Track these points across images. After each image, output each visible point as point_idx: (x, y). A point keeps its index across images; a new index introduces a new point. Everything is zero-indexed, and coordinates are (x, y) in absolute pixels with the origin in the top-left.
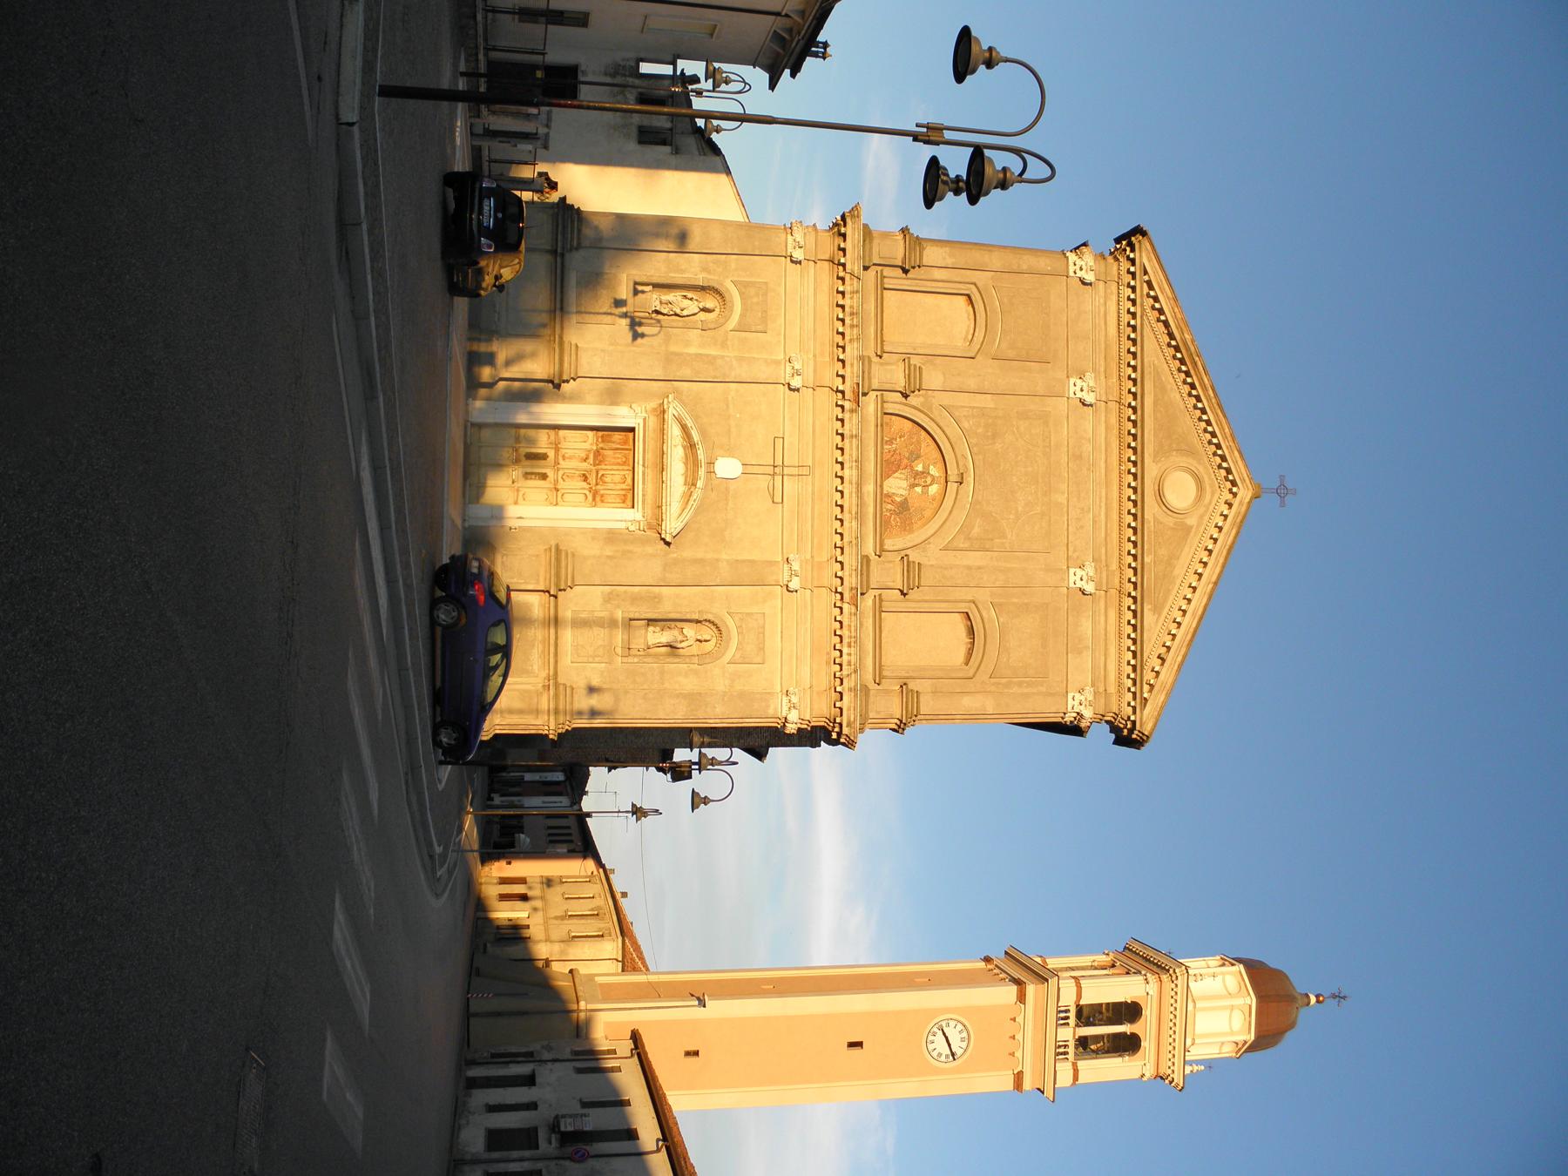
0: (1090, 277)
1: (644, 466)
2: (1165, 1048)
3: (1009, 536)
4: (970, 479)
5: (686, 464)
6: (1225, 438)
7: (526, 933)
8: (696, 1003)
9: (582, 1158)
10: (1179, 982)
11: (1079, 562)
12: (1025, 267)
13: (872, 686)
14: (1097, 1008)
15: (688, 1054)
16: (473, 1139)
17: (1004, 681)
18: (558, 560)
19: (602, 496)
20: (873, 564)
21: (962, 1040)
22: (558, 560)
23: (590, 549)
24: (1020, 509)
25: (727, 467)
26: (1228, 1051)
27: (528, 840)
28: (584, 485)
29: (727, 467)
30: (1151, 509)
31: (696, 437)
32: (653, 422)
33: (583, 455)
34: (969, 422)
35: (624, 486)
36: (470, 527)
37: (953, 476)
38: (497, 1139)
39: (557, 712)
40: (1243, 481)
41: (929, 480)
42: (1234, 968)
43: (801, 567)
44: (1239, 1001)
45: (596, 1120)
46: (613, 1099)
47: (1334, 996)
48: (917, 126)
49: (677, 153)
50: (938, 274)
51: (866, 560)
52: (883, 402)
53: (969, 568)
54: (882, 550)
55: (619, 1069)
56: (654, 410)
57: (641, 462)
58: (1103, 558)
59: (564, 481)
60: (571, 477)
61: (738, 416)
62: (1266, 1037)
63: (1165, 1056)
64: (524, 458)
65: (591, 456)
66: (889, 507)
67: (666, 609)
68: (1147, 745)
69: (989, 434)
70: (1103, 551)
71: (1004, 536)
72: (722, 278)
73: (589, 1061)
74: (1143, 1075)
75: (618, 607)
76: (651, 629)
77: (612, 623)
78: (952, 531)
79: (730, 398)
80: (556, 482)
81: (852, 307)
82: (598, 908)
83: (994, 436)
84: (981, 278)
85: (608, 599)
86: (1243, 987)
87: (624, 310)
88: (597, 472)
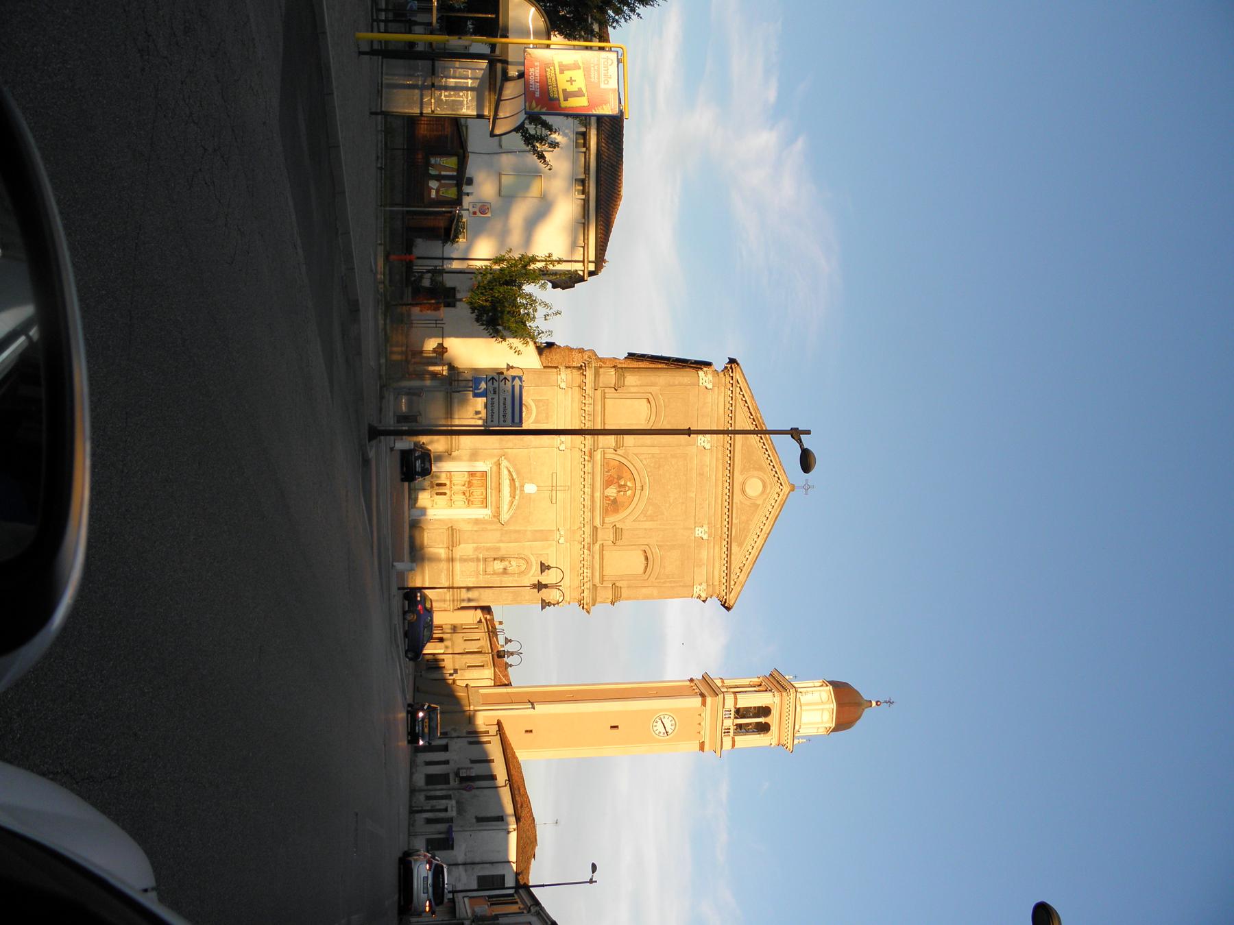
0: (710, 386)
2: (784, 730)
5: (511, 488)
6: (777, 463)
7: (442, 664)
8: (531, 706)
9: (469, 789)
10: (791, 696)
11: (701, 525)
12: (677, 383)
13: (598, 585)
14: (747, 709)
15: (527, 731)
16: (420, 780)
17: (662, 581)
18: (452, 534)
20: (599, 530)
21: (672, 725)
22: (452, 534)
23: (467, 527)
25: (530, 488)
26: (822, 731)
27: (469, 23)
28: (464, 496)
29: (530, 488)
30: (738, 497)
31: (515, 476)
32: (495, 468)
33: (463, 483)
35: (482, 497)
36: (412, 520)
37: (638, 487)
38: (431, 779)
39: (453, 601)
40: (785, 483)
41: (627, 488)
42: (828, 688)
43: (565, 533)
44: (827, 706)
45: (477, 770)
46: (485, 759)
47: (886, 702)
48: (450, 796)
50: (633, 389)
51: (595, 529)
52: (604, 454)
53: (645, 529)
54: (603, 523)
55: (489, 742)
56: (495, 463)
58: (713, 522)
62: (843, 723)
63: (783, 734)
66: (608, 502)
67: (502, 553)
68: (732, 610)
70: (713, 519)
73: (474, 737)
74: (771, 744)
75: (480, 553)
76: (496, 562)
77: (478, 560)
78: (637, 512)
80: (451, 496)
81: (588, 411)
82: (482, 647)
84: (653, 389)
85: (476, 549)
86: (830, 699)
87: (480, 416)
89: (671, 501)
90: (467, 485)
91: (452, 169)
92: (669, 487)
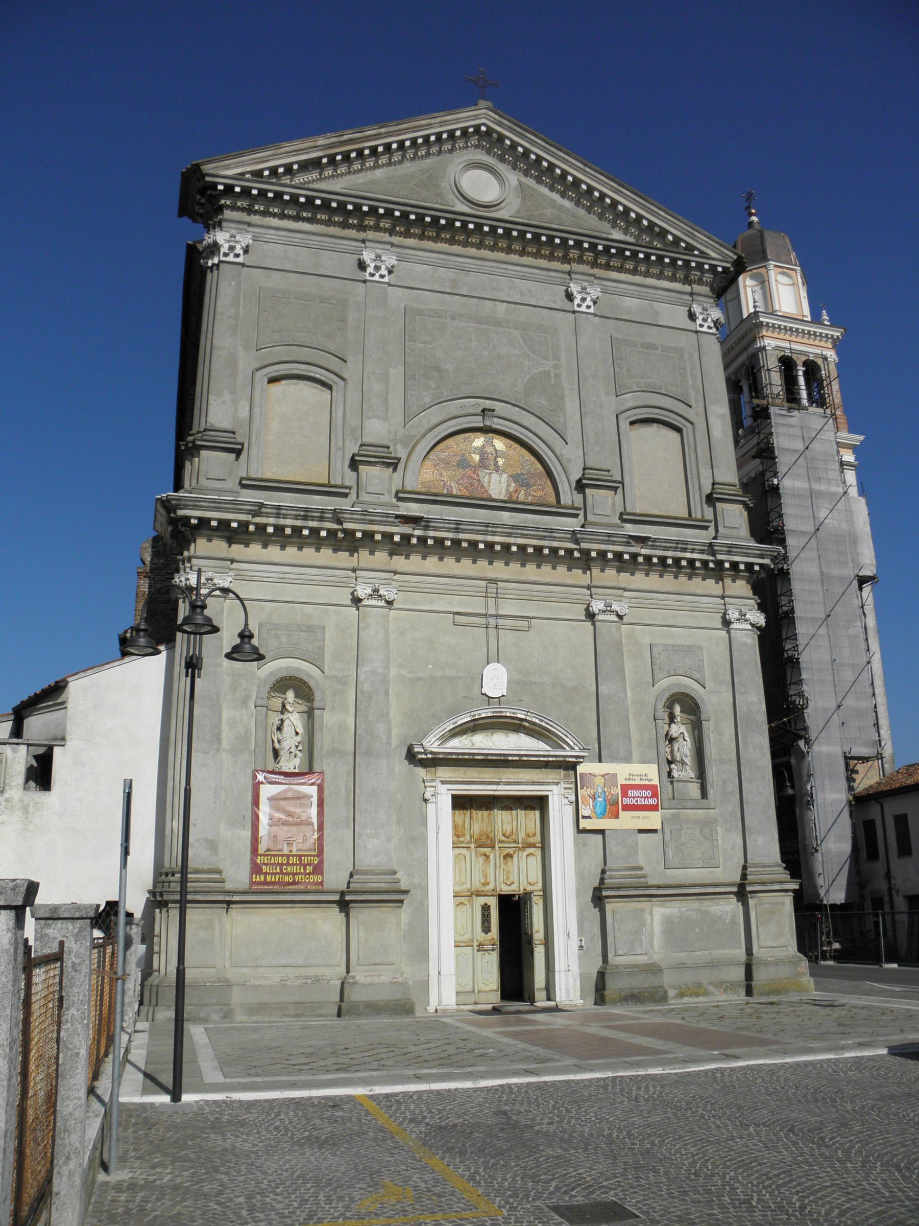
1: (498, 783)
3: (547, 368)
4: (488, 404)
19: (528, 835)
24: (517, 352)
28: (515, 856)
32: (444, 773)
33: (481, 859)
34: (424, 396)
41: (489, 450)
49: (63, 739)
57: (494, 787)
59: (513, 883)
60: (508, 874)
61: (430, 666)
64: (489, 934)
65: (482, 850)
69: (436, 374)
71: (547, 373)
72: (256, 681)
79: (410, 676)
83: (439, 370)
88: (500, 842)
89: (517, 352)
90: (487, 850)
91: (608, 903)
92: (485, 353)
